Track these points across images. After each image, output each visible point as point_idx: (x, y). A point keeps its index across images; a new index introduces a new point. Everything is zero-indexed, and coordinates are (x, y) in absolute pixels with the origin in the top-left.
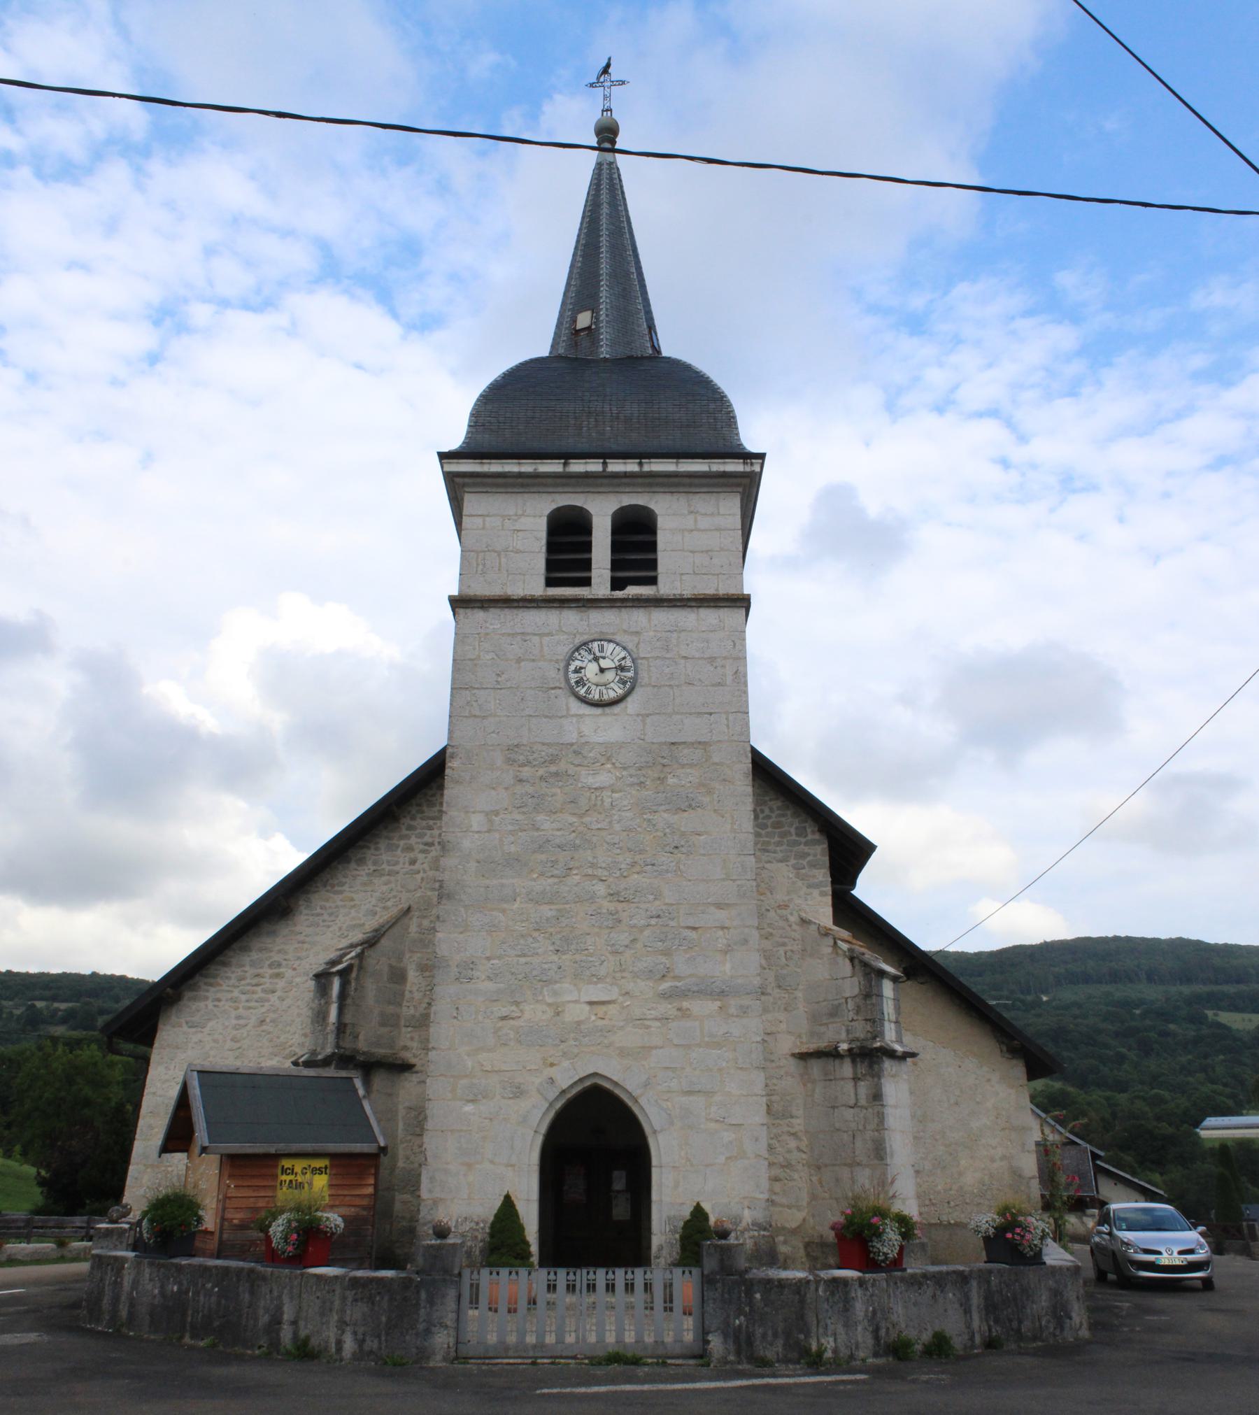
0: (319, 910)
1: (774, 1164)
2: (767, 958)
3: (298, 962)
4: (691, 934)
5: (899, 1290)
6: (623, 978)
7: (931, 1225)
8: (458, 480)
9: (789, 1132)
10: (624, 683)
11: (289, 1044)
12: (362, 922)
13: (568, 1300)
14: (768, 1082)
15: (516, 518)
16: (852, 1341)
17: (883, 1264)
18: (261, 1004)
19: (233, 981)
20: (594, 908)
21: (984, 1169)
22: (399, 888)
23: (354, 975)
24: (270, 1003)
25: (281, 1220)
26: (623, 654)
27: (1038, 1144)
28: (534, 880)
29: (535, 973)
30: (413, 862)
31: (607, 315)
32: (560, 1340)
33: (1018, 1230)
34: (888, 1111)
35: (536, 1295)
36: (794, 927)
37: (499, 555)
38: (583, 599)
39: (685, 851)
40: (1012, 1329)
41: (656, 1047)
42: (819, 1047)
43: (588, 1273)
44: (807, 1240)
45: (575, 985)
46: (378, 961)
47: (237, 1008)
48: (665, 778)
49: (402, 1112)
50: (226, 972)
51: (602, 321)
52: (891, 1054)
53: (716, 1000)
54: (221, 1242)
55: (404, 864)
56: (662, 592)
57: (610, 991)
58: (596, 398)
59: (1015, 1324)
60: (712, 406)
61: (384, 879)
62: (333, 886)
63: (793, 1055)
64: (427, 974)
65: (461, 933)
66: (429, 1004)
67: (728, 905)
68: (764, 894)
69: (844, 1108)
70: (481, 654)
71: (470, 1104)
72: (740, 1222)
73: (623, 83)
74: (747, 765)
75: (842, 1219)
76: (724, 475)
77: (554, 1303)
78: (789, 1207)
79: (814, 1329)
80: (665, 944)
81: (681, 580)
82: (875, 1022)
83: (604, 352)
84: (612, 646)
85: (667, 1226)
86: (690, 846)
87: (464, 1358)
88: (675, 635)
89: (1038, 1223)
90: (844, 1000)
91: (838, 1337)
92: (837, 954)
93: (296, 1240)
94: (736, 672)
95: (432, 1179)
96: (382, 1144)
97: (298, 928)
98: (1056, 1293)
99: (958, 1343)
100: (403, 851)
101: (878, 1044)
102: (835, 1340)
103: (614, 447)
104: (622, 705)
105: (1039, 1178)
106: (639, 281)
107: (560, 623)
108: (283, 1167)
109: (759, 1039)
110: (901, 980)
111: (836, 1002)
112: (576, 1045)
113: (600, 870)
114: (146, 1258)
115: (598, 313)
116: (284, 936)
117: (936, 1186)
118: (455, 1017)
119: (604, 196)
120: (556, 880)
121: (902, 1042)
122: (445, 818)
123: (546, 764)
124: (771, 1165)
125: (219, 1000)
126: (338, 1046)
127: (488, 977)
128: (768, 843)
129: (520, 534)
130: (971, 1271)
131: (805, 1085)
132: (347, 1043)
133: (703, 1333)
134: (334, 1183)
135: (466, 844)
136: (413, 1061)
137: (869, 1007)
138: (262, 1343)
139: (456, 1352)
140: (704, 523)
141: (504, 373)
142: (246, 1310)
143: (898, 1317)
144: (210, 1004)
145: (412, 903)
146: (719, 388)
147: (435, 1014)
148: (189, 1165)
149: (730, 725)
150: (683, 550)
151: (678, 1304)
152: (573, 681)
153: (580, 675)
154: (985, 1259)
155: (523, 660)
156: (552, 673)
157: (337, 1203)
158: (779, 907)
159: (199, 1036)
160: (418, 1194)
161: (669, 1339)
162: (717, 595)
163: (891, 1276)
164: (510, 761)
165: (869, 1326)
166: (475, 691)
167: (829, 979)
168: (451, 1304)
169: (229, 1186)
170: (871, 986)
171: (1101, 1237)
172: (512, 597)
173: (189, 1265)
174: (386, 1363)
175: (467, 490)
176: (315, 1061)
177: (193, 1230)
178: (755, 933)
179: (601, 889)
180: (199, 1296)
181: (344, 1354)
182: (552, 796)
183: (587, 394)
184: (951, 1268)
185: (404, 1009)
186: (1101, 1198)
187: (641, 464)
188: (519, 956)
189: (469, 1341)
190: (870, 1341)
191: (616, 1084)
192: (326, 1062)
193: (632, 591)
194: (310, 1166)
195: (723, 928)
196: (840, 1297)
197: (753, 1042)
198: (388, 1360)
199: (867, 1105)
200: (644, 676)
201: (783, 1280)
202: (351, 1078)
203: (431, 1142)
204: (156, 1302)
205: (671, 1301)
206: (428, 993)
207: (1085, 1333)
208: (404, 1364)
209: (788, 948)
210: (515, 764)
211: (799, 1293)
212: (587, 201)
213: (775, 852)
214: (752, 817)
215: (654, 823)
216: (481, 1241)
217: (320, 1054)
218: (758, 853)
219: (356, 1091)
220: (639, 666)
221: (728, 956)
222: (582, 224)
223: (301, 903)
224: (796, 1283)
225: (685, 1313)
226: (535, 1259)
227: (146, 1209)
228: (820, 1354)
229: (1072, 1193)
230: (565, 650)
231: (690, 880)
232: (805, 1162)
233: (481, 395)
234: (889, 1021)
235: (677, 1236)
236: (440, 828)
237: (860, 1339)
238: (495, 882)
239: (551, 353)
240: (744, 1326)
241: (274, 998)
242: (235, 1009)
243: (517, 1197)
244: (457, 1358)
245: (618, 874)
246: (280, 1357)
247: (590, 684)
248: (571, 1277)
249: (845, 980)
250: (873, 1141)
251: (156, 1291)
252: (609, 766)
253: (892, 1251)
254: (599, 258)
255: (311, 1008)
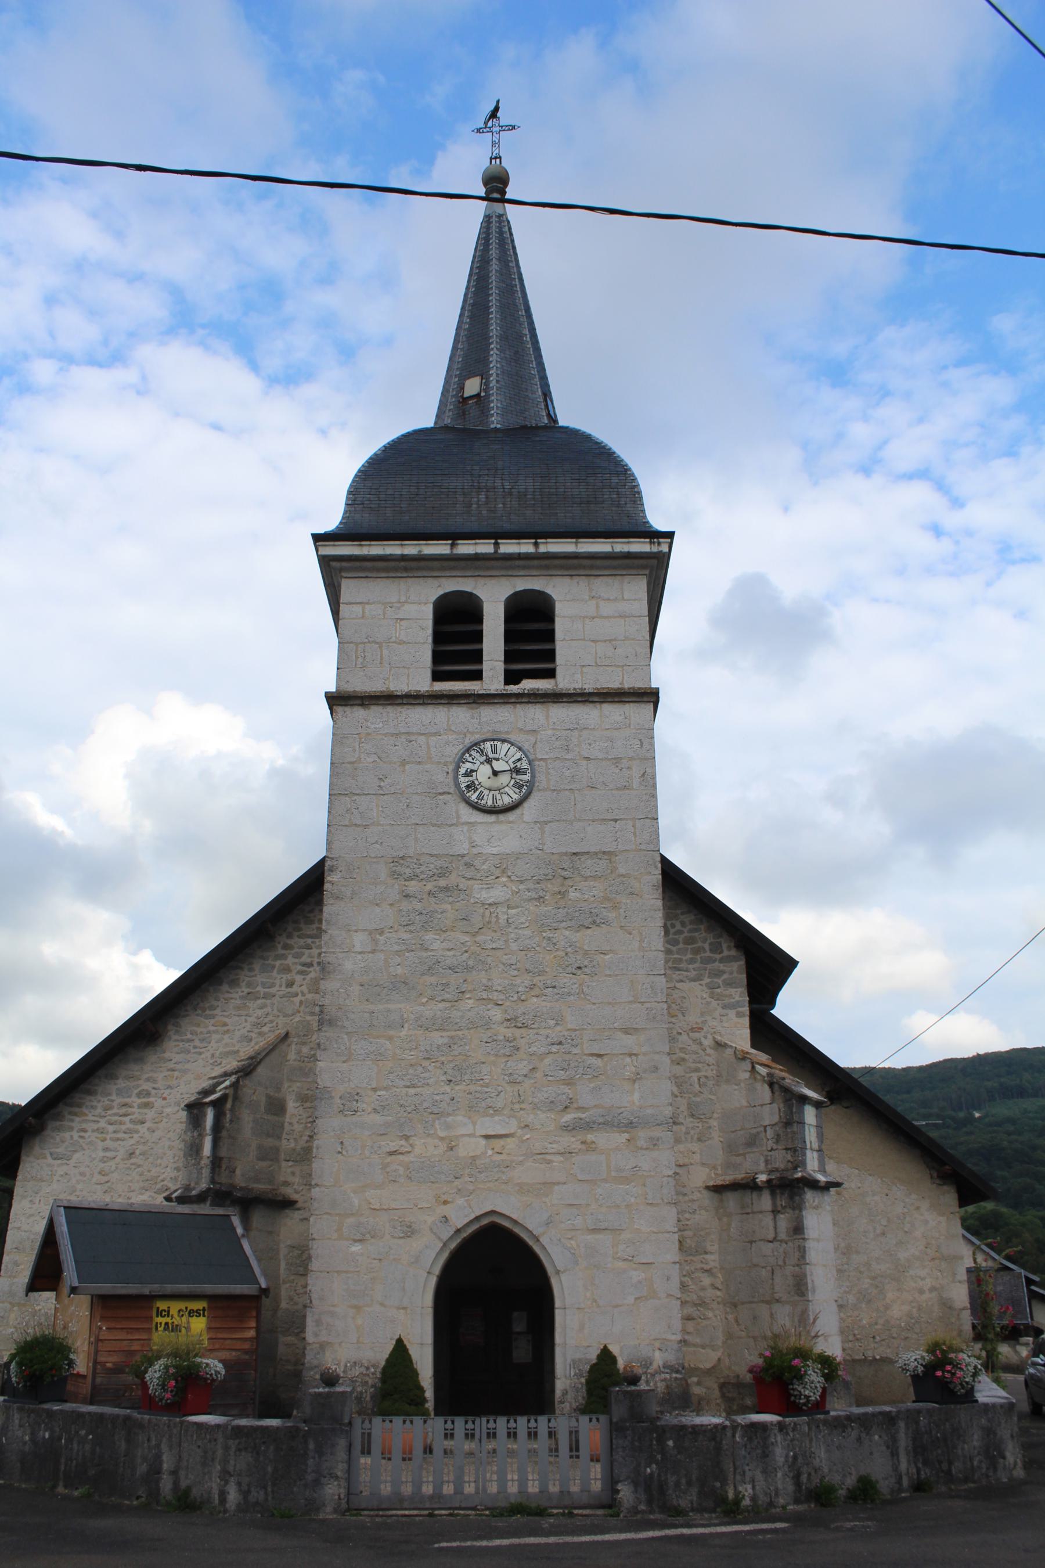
0: (189, 1036)
1: (686, 1302)
2: (679, 1085)
3: (168, 1091)
4: (596, 1062)
5: (822, 1434)
6: (521, 1109)
7: (854, 1361)
8: (334, 564)
9: (702, 1269)
10: (520, 787)
11: (161, 1178)
12: (236, 1049)
13: (466, 1447)
14: (680, 1216)
15: (399, 605)
16: (772, 1488)
17: (804, 1408)
18: (131, 1135)
19: (99, 1111)
20: (490, 1035)
21: (912, 1302)
22: (275, 1012)
23: (229, 1105)
24: (140, 1135)
25: (159, 1365)
26: (518, 755)
27: (969, 1271)
28: (423, 1004)
29: (425, 1105)
30: (290, 984)
31: (498, 382)
32: (458, 1491)
33: (949, 1368)
34: (810, 1245)
35: (431, 1443)
36: (709, 1051)
37: (380, 647)
38: (474, 695)
39: (589, 972)
40: (943, 1471)
41: (559, 1183)
42: (735, 1179)
43: (488, 1421)
44: (722, 1380)
45: (470, 1118)
46: (254, 1091)
47: (104, 1140)
48: (567, 891)
49: (283, 1251)
50: (90, 1101)
51: (492, 388)
52: (813, 1185)
53: (624, 1132)
54: (94, 1387)
55: (281, 986)
56: (561, 686)
57: (508, 1123)
58: (486, 472)
59: (945, 1466)
60: (615, 480)
61: (259, 1002)
62: (204, 1010)
63: (708, 1188)
64: (308, 1104)
65: (344, 1062)
66: (311, 1137)
67: (636, 1030)
68: (677, 1016)
69: (762, 1242)
70: (362, 756)
71: (356, 1244)
72: (651, 1364)
73: (513, 128)
74: (656, 876)
75: (760, 1361)
76: (629, 556)
77: (451, 1452)
78: (703, 1347)
79: (731, 1477)
80: (568, 1073)
81: (582, 672)
82: (797, 1151)
83: (495, 422)
84: (506, 746)
85: (572, 1369)
86: (594, 966)
87: (356, 1510)
88: (576, 733)
89: (969, 1358)
90: (762, 1129)
91: (756, 1484)
92: (755, 1079)
93: (175, 1387)
94: (643, 775)
95: (318, 1322)
96: (264, 1286)
97: (167, 1055)
98: (989, 1432)
99: (884, 1486)
100: (279, 972)
101: (800, 1175)
102: (754, 1488)
103: (507, 526)
104: (518, 812)
105: (971, 1309)
106: (532, 344)
107: (448, 720)
108: (158, 1308)
109: (670, 1173)
110: (824, 1105)
111: (754, 1131)
112: (471, 1182)
113: (496, 994)
114: (15, 1403)
115: (487, 379)
116: (152, 1064)
117: (860, 1320)
118: (339, 1152)
119: (494, 252)
120: (448, 1005)
121: (825, 1172)
122: (325, 937)
123: (435, 878)
124: (683, 1303)
125: (85, 1131)
126: (213, 1181)
127: (374, 1109)
128: (681, 960)
129: (403, 623)
130: (899, 1412)
131: (720, 1219)
132: (223, 1179)
133: (612, 1482)
134: (213, 1325)
135: (348, 965)
136: (295, 1197)
137: (790, 1136)
138: (140, 1493)
139: (348, 1504)
140: (607, 609)
141: (384, 446)
142: (122, 1459)
143: (821, 1461)
144: (76, 1135)
145: (289, 1029)
146: (622, 461)
147: (318, 1149)
148: (58, 1306)
149: (638, 834)
150: (584, 640)
151: (584, 1452)
152: (463, 786)
153: (471, 779)
154: (914, 1399)
155: (408, 763)
156: (440, 777)
157: (217, 1346)
158: (692, 1030)
159: (65, 1168)
160: (303, 1336)
161: (575, 1488)
162: (623, 689)
163: (813, 1419)
164: (395, 875)
165: (790, 1471)
166: (356, 797)
167: (747, 1107)
168: (341, 1454)
169: (101, 1328)
170: (792, 1112)
171: (1037, 1370)
172: (395, 693)
173: (61, 1410)
174: (273, 1515)
175: (344, 574)
176: (190, 1196)
177: (64, 1374)
178: (667, 1060)
179: (497, 1014)
180: (72, 1444)
181: (227, 1505)
182: (442, 913)
183: (477, 467)
184: (878, 1409)
185: (284, 1142)
186: (1035, 1324)
187: (536, 544)
188: (408, 1087)
189: (361, 1492)
190: (791, 1488)
191: (516, 1222)
192: (201, 1198)
193: (528, 685)
194: (186, 1308)
195: (630, 1055)
196: (758, 1442)
197: (665, 1176)
198: (275, 1512)
199: (787, 1238)
200: (541, 779)
201: (697, 1426)
202: (228, 1216)
203: (316, 1284)
204: (27, 1448)
205: (577, 1450)
206: (309, 1125)
207: (1019, 1473)
208: (292, 1516)
209: (700, 1074)
210: (401, 878)
211: (714, 1439)
212: (474, 257)
213: (687, 971)
214: (663, 933)
215: (555, 941)
216: (372, 1386)
217: (194, 1189)
218: (669, 972)
219: (234, 1229)
220: (536, 768)
221: (637, 1085)
222: (469, 281)
223: (170, 1027)
224: (711, 1430)
225: (592, 1460)
226: (430, 1405)
227: (14, 1351)
228: (737, 1502)
229: (1005, 1322)
230: (456, 750)
231: (594, 1004)
232: (719, 1300)
233: (360, 471)
234: (811, 1149)
235: (583, 1380)
236: (320, 947)
237: (780, 1486)
238: (381, 1007)
239: (435, 423)
240: (656, 1475)
241: (143, 1129)
242: (103, 1141)
243: (409, 1341)
244: (348, 1510)
245: (515, 998)
246: (159, 1508)
247: (482, 789)
248: (470, 1425)
249: (764, 1107)
250: (793, 1276)
251: (27, 1438)
252: (504, 879)
253: (814, 1393)
254: (488, 319)
255: (183, 1140)
